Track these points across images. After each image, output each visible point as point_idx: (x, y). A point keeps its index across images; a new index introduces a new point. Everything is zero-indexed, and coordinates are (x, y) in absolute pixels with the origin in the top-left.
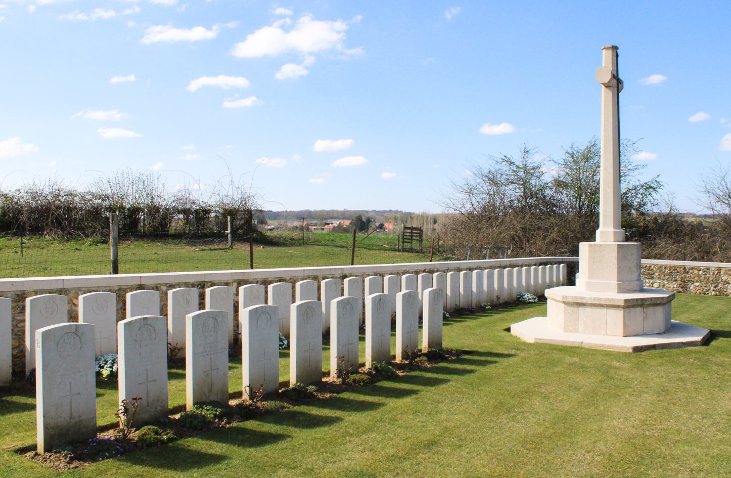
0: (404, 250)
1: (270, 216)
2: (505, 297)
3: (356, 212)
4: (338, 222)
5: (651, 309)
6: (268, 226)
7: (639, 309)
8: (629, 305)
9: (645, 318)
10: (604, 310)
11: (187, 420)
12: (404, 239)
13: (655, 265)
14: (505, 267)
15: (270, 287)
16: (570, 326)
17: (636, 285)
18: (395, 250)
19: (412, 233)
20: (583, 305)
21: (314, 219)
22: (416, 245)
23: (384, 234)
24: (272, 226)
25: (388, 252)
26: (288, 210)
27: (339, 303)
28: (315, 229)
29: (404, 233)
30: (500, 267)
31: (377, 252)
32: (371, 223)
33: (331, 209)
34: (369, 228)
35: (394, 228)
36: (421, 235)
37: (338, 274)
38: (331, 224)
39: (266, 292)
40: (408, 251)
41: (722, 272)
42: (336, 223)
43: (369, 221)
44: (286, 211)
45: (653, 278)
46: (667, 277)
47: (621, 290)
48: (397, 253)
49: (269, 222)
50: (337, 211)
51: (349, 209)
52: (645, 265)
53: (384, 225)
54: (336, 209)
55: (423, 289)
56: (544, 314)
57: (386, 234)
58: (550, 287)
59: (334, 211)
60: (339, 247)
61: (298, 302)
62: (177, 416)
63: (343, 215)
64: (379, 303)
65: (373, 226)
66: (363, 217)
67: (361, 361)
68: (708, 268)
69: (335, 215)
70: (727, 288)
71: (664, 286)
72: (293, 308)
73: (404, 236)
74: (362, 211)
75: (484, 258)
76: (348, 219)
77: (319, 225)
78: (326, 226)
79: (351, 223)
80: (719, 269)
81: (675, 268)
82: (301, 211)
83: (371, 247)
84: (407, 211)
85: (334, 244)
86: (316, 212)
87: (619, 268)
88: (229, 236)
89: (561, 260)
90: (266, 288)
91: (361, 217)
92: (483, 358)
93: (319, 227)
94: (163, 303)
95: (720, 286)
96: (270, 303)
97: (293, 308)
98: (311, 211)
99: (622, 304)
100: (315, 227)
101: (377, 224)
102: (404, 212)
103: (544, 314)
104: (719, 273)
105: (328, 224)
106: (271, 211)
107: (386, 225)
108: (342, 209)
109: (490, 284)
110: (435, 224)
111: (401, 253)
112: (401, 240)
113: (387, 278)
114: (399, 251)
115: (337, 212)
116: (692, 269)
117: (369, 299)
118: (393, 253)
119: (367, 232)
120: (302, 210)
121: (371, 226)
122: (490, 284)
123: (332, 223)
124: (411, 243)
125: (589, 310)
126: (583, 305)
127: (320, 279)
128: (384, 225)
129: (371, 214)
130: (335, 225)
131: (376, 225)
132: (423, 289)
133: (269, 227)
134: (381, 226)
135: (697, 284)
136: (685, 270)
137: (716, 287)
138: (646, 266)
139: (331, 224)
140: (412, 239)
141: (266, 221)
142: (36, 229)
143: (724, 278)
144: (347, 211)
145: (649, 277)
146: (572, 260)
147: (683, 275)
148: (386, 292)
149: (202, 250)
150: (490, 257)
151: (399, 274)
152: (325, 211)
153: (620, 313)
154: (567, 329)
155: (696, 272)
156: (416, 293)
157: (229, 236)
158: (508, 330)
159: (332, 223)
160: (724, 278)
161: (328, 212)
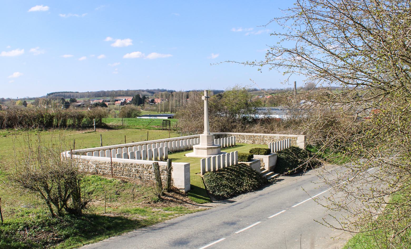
0: (163, 129)
2: (178, 149)
3: (135, 91)
4: (124, 99)
8: (208, 149)
9: (212, 151)
10: (203, 150)
12: (163, 125)
15: (128, 148)
17: (212, 144)
18: (160, 130)
20: (199, 149)
21: (108, 96)
23: (155, 106)
25: (157, 130)
26: (89, 91)
28: (108, 104)
29: (163, 122)
31: (153, 130)
32: (146, 99)
36: (170, 123)
37: (145, 144)
38: (119, 101)
40: (165, 130)
41: (265, 137)
42: (123, 99)
43: (144, 98)
44: (88, 92)
48: (161, 131)
50: (123, 91)
58: (194, 145)
59: (121, 91)
63: (127, 93)
65: (147, 101)
66: (140, 95)
69: (122, 93)
72: (142, 151)
73: (163, 124)
75: (187, 135)
76: (130, 96)
77: (112, 102)
78: (116, 102)
79: (132, 100)
80: (264, 136)
81: (251, 136)
82: (98, 92)
85: (135, 128)
86: (108, 92)
87: (207, 140)
88: (94, 126)
89: (137, 144)
91: (139, 95)
95: (264, 141)
98: (105, 92)
100: (109, 103)
101: (150, 100)
102: (167, 90)
104: (264, 137)
105: (117, 100)
107: (156, 100)
108: (126, 90)
109: (220, 141)
111: (162, 131)
112: (162, 126)
114: (161, 130)
117: (148, 150)
121: (146, 102)
122: (220, 141)
123: (120, 100)
124: (166, 126)
125: (200, 150)
126: (199, 149)
129: (145, 93)
133: (78, 104)
134: (153, 101)
139: (119, 101)
140: (166, 125)
143: (265, 139)
144: (129, 91)
148: (156, 148)
149: (86, 133)
150: (189, 135)
151: (159, 143)
152: (114, 91)
153: (206, 150)
154: (196, 154)
157: (94, 126)
158: (185, 155)
159: (120, 100)
160: (265, 139)
161: (116, 92)
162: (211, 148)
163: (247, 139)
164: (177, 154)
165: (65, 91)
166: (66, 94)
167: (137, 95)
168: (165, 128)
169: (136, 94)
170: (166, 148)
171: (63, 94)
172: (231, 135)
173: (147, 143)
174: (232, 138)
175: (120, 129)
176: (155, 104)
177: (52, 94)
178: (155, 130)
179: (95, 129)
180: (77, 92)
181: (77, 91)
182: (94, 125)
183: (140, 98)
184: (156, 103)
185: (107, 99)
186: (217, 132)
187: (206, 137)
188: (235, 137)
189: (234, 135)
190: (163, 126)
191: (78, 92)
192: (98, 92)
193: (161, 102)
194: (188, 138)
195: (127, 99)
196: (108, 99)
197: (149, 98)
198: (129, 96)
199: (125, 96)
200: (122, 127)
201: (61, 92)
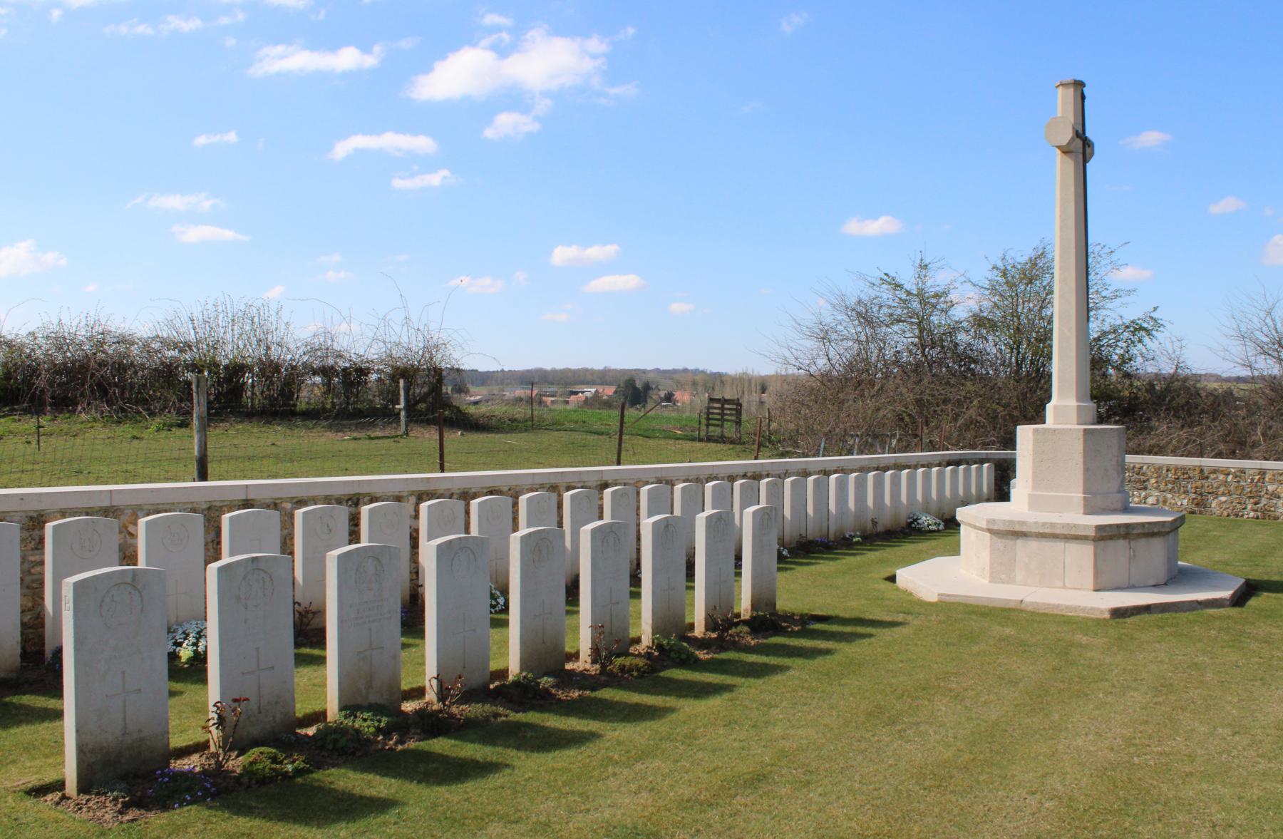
0: (709, 439)
2: (885, 521)
3: (624, 372)
4: (593, 390)
5: (1143, 542)
8: (1105, 535)
10: (1060, 545)
12: (708, 419)
13: (1149, 465)
14: (886, 469)
16: (1000, 572)
18: (693, 439)
19: (722, 408)
21: (552, 384)
22: (729, 430)
24: (478, 397)
28: (552, 402)
29: (709, 408)
30: (877, 469)
31: (662, 442)
32: (651, 392)
36: (739, 412)
37: (592, 481)
39: (467, 513)
40: (716, 441)
43: (647, 387)
45: (1145, 489)
46: (1170, 486)
47: (1090, 509)
48: (697, 444)
49: (473, 389)
52: (1132, 465)
54: (590, 367)
55: (743, 507)
56: (955, 550)
61: (524, 531)
62: (311, 731)
63: (603, 377)
64: (664, 532)
67: (633, 634)
68: (1243, 471)
69: (589, 377)
70: (1275, 506)
72: (515, 539)
73: (708, 413)
74: (635, 370)
75: (850, 452)
77: (561, 396)
78: (573, 398)
79: (616, 392)
80: (1263, 473)
81: (1185, 470)
84: (715, 370)
86: (554, 371)
87: (1086, 470)
88: (403, 413)
90: (468, 505)
91: (634, 381)
92: (848, 629)
93: (561, 399)
94: (286, 532)
95: (1264, 501)
96: (474, 531)
99: (1092, 533)
100: (553, 399)
101: (662, 394)
102: (708, 372)
103: (955, 550)
104: (1262, 479)
105: (576, 393)
106: (476, 371)
107: (678, 395)
111: (703, 444)
112: (704, 421)
113: (679, 487)
114: (700, 440)
115: (592, 372)
116: (1215, 471)
117: (647, 523)
118: (689, 443)
120: (530, 368)
123: (583, 392)
124: (722, 426)
125: (1033, 544)
127: (562, 489)
128: (674, 395)
129: (650, 377)
130: (588, 394)
132: (743, 506)
133: (472, 399)
134: (669, 397)
135: (1223, 499)
136: (1203, 474)
137: (1256, 504)
138: (1134, 467)
140: (723, 420)
143: (1271, 488)
144: (609, 370)
145: (1138, 485)
146: (1002, 457)
149: (355, 439)
150: (861, 452)
152: (570, 370)
154: (994, 578)
155: (1221, 477)
157: (403, 413)
158: (892, 579)
159: (583, 392)
160: (1271, 488)
161: (575, 372)
162: (1126, 532)
163: (1162, 486)
164: (825, 567)
167: (629, 380)
168: (715, 431)
169: (627, 377)
170: (763, 520)
173: (606, 478)
175: (521, 432)
176: (674, 404)
178: (671, 442)
182: (401, 406)
183: (635, 388)
184: (678, 401)
185: (548, 390)
187: (1078, 446)
190: (708, 425)
192: (528, 371)
193: (692, 401)
195: (601, 391)
196: (552, 389)
197: (659, 390)
198: (607, 384)
199: (599, 384)
200: (529, 423)
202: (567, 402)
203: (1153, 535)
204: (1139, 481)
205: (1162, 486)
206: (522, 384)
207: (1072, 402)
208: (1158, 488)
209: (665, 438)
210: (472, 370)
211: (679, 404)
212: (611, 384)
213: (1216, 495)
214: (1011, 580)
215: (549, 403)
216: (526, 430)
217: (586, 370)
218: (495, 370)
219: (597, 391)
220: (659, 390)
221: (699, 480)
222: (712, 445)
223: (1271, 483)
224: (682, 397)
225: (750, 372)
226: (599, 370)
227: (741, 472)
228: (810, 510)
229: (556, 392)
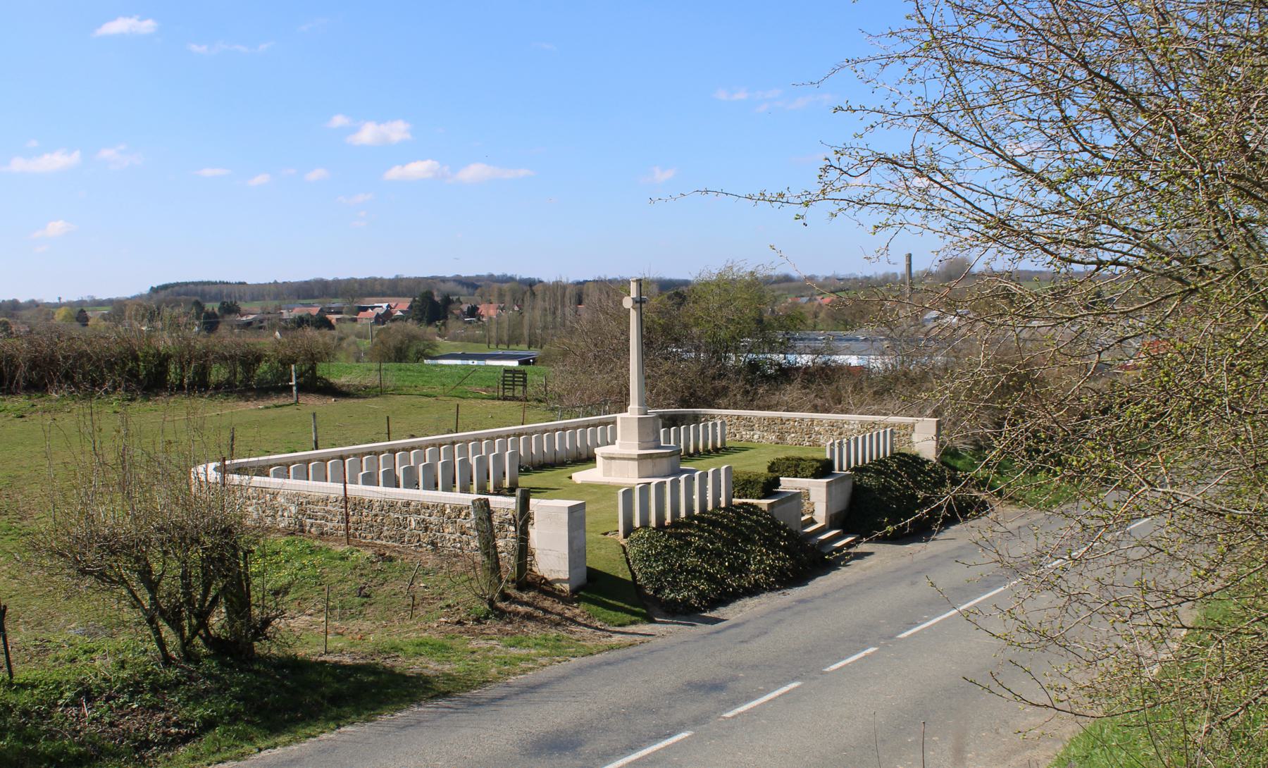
0: (505, 399)
1: (242, 295)
3: (419, 281)
4: (385, 305)
5: (658, 460)
6: (242, 316)
7: (649, 460)
9: (654, 466)
11: (645, 333)
12: (504, 385)
13: (754, 417)
14: (588, 426)
16: (606, 472)
17: (652, 444)
18: (493, 399)
19: (514, 377)
21: (336, 296)
22: (519, 392)
24: (251, 317)
26: (280, 281)
27: (424, 466)
28: (337, 319)
29: (504, 377)
30: (593, 426)
31: (473, 401)
32: (451, 307)
33: (367, 277)
34: (449, 316)
35: (499, 316)
38: (370, 310)
41: (815, 423)
43: (447, 301)
45: (753, 430)
46: (766, 428)
47: (640, 448)
48: (497, 402)
49: (244, 306)
50: (381, 279)
51: (406, 276)
53: (478, 309)
54: (379, 277)
55: (473, 456)
56: (595, 467)
57: (483, 326)
59: (375, 280)
60: (426, 396)
61: (442, 461)
63: (394, 288)
64: (480, 461)
66: (435, 293)
68: (803, 420)
69: (378, 288)
70: (819, 439)
71: (763, 438)
72: (440, 463)
73: (504, 381)
74: (433, 278)
78: (362, 314)
79: (411, 307)
80: (812, 420)
81: (773, 419)
83: (464, 395)
84: (525, 276)
85: (418, 393)
86: (337, 282)
87: (639, 433)
88: (294, 388)
91: (432, 294)
93: (347, 316)
95: (813, 436)
97: (440, 463)
99: (636, 457)
101: (465, 307)
102: (518, 278)
103: (595, 467)
104: (812, 424)
105: (365, 309)
107: (483, 309)
110: (580, 304)
111: (501, 402)
112: (501, 386)
113: (484, 443)
114: (499, 399)
115: (382, 281)
116: (788, 420)
117: (457, 459)
118: (491, 402)
119: (444, 324)
120: (307, 279)
123: (373, 308)
124: (514, 389)
128: (478, 309)
129: (450, 287)
130: (377, 310)
131: (461, 310)
132: (473, 456)
134: (473, 311)
135: (793, 435)
136: (782, 421)
137: (809, 438)
139: (370, 310)
141: (237, 307)
142: (36, 386)
143: (817, 429)
144: (402, 280)
145: (749, 428)
147: (780, 427)
149: (267, 408)
152: (355, 280)
155: (792, 423)
156: (468, 459)
157: (294, 388)
158: (571, 478)
159: (373, 308)
160: (817, 429)
161: (362, 283)
163: (762, 428)
165: (205, 279)
166: (206, 287)
167: (426, 293)
169: (423, 289)
171: (200, 288)
172: (713, 417)
174: (715, 425)
175: (374, 397)
176: (479, 320)
177: (165, 287)
178: (479, 401)
179: (295, 396)
180: (240, 283)
181: (242, 281)
182: (294, 383)
183: (434, 303)
184: (483, 316)
185: (334, 306)
186: (668, 406)
187: (636, 424)
188: (723, 424)
189: (722, 415)
190: (504, 389)
191: (244, 283)
192: (306, 282)
194: (582, 424)
195: (393, 305)
197: (461, 303)
198: (399, 296)
201: (193, 283)
202: (355, 320)
203: (662, 457)
204: (750, 426)
205: (762, 428)
206: (299, 298)
207: (637, 407)
208: (759, 430)
209: (475, 398)
210: (240, 283)
211: (484, 319)
212: (404, 295)
213: (790, 434)
214: (610, 476)
215: (334, 321)
216: (377, 396)
217: (374, 280)
218: (268, 282)
219: (389, 306)
220: (461, 303)
221: (492, 438)
222: (508, 402)
223: (817, 425)
224: (489, 311)
225: (564, 280)
226: (390, 280)
227: (513, 433)
228: (557, 448)
229: (343, 308)
